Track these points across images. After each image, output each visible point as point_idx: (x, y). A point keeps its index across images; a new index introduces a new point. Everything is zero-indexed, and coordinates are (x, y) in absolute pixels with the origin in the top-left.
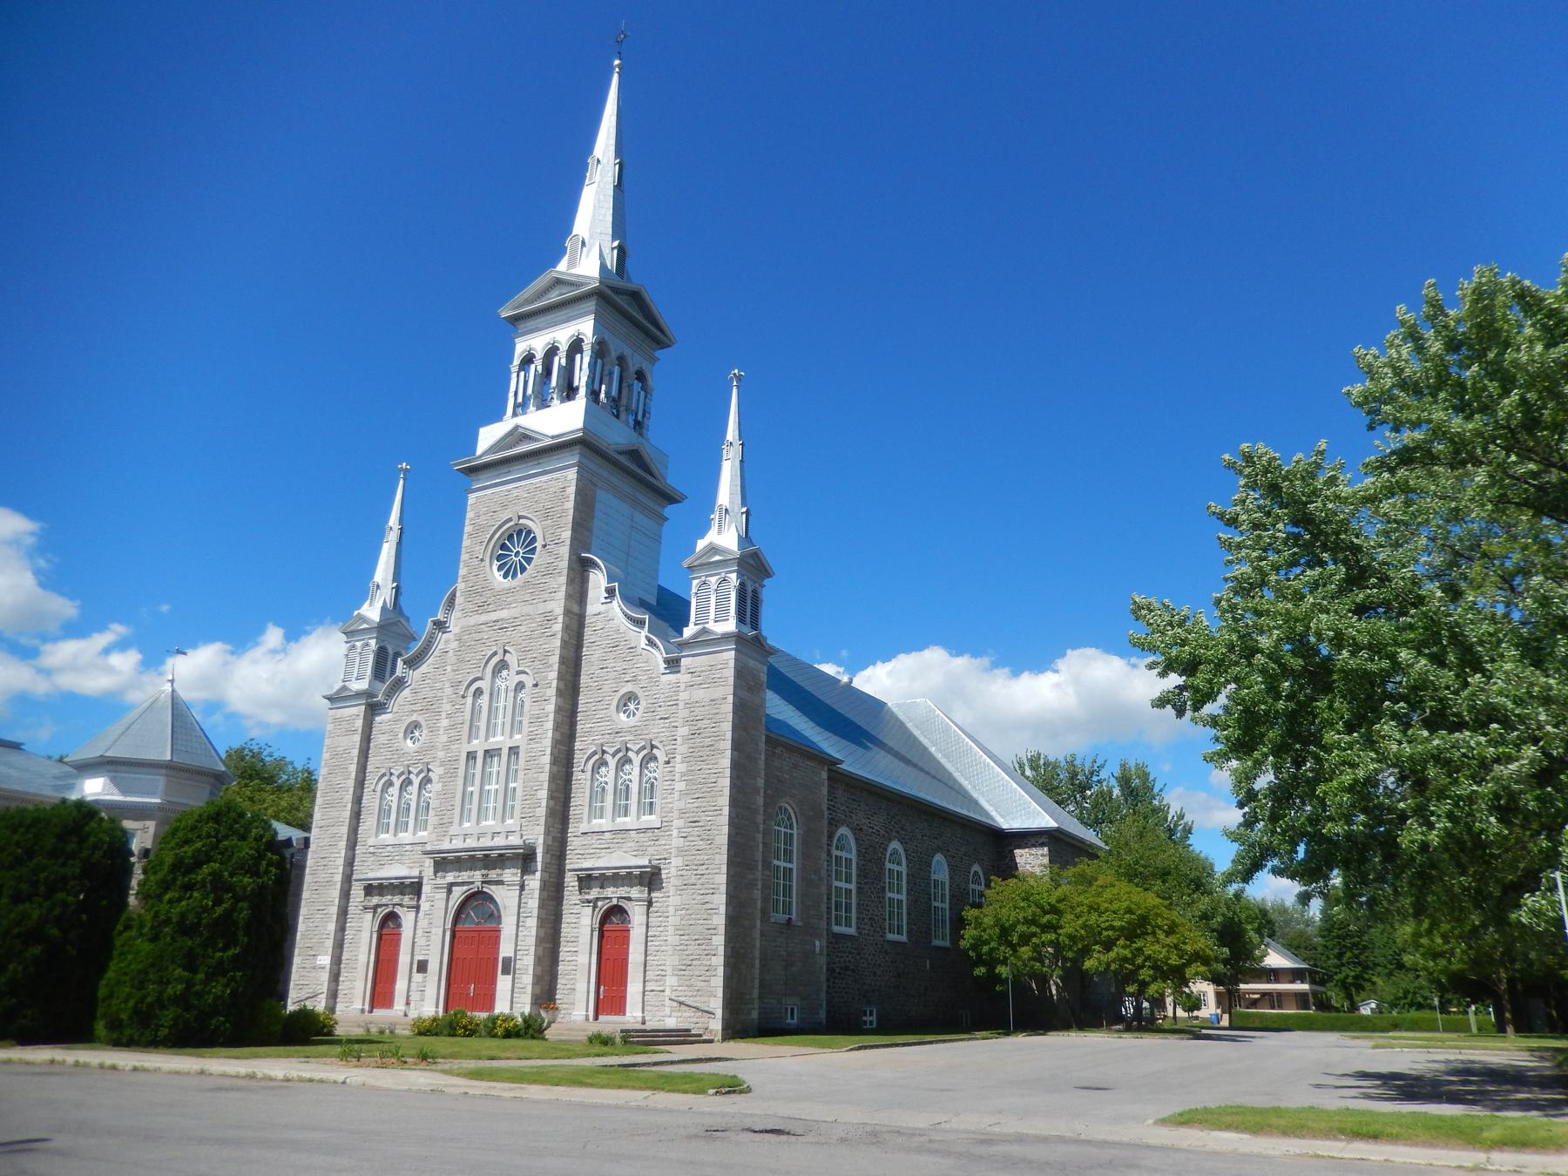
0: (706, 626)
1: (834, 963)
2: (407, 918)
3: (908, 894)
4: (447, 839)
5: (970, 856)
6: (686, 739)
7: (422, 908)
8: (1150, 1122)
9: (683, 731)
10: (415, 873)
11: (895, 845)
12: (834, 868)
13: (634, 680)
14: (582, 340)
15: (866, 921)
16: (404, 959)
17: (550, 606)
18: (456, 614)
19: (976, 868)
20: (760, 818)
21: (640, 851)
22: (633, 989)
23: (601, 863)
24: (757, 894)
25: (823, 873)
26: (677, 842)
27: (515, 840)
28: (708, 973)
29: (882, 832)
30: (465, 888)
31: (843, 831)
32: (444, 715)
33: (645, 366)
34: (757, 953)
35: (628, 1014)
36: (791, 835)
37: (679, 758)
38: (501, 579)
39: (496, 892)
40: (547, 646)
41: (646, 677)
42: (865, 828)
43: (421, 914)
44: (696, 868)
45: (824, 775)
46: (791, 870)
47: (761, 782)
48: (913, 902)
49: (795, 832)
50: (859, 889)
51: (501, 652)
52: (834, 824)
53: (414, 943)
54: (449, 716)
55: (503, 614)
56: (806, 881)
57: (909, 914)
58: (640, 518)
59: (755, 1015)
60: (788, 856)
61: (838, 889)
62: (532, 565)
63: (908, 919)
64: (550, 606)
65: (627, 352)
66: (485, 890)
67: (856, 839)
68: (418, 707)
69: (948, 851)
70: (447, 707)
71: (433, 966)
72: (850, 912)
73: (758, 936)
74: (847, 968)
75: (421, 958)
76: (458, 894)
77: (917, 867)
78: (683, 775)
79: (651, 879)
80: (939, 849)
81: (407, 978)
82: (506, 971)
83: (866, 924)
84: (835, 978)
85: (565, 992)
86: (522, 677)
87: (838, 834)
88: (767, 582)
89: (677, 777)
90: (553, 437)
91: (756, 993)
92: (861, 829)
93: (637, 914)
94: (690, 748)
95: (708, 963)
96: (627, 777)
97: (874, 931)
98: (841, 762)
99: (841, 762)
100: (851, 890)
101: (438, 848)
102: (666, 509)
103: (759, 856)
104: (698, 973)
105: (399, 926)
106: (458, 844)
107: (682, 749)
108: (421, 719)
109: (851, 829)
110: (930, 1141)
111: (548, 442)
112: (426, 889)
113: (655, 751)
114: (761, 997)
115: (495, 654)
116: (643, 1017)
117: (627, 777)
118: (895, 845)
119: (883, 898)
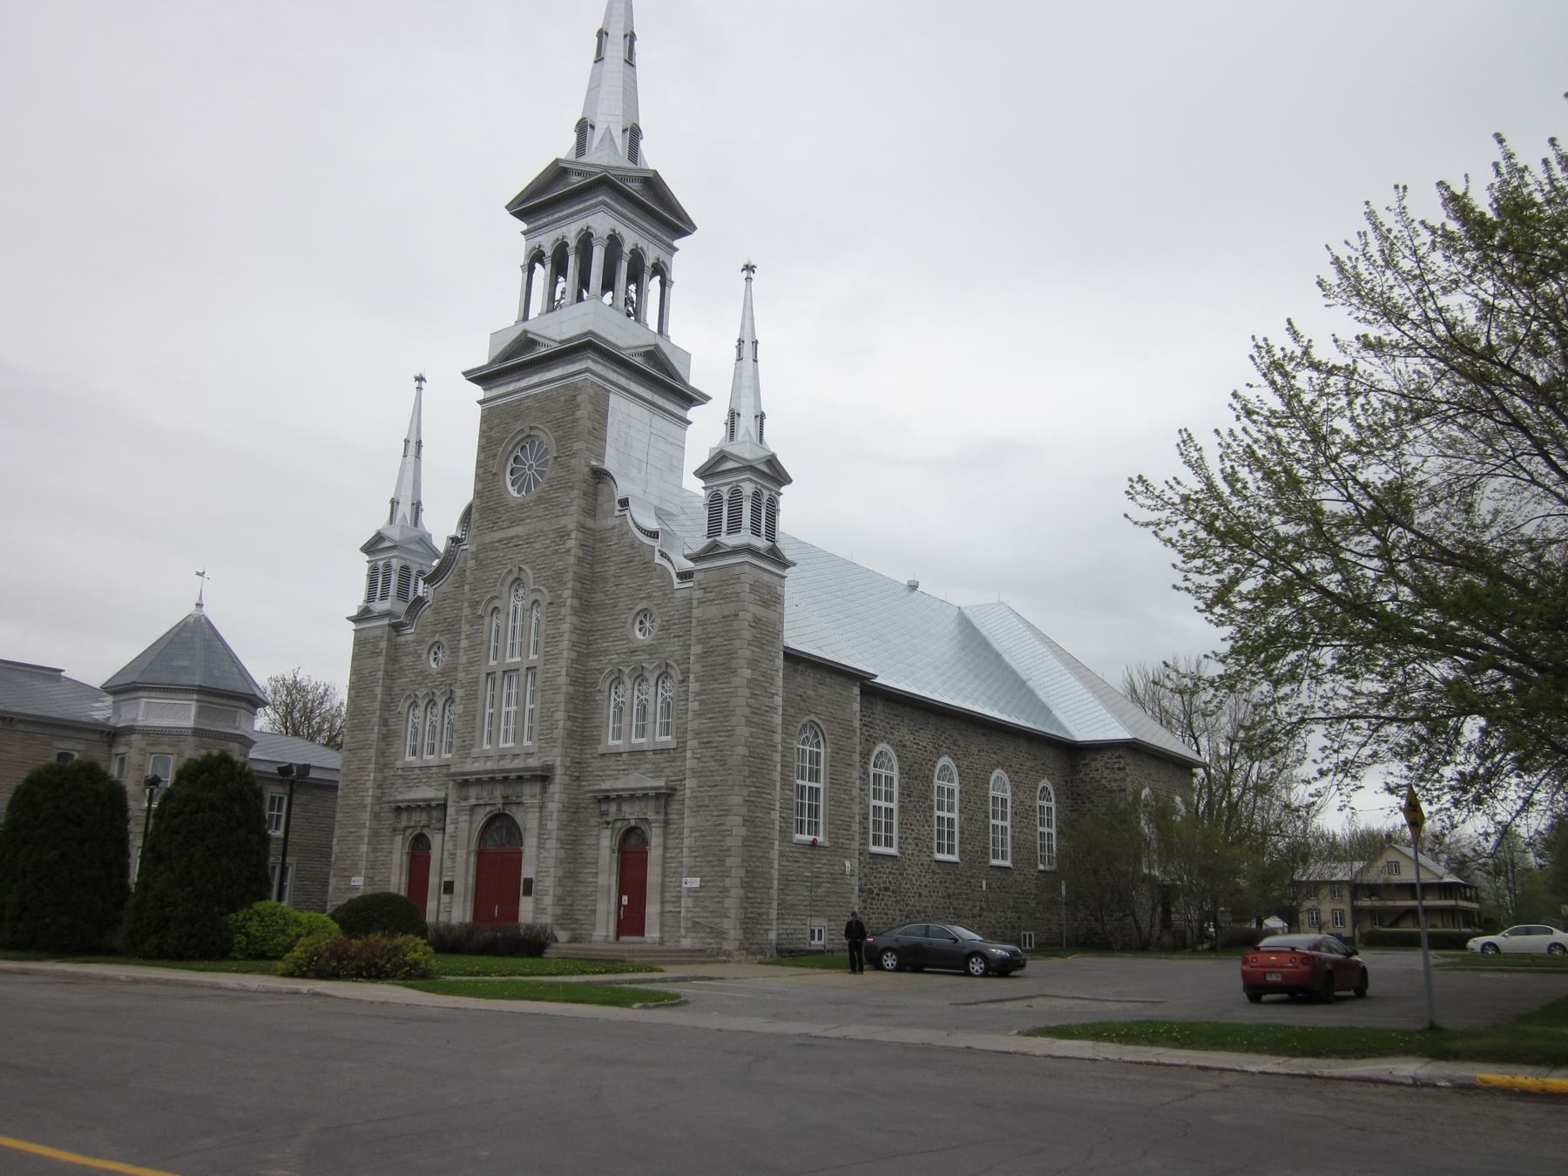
0: (718, 538)
1: (872, 884)
2: (436, 841)
3: (961, 811)
4: (469, 761)
5: (1037, 771)
6: (700, 658)
7: (447, 831)
8: (1015, 1032)
9: (696, 649)
10: (442, 794)
11: (945, 760)
12: (872, 787)
13: (649, 597)
14: (567, 244)
15: (910, 840)
16: (433, 880)
17: (564, 521)
18: (1466, 311)
19: (1045, 783)
20: (778, 738)
21: (657, 772)
22: (652, 910)
23: (619, 784)
24: (775, 815)
25: (855, 792)
26: (690, 763)
27: (533, 762)
28: (721, 895)
29: (930, 748)
30: (488, 809)
31: (882, 747)
32: (463, 636)
33: (663, 257)
34: (775, 874)
35: (646, 935)
36: (818, 754)
37: (692, 677)
38: (515, 494)
39: (518, 815)
40: (561, 563)
41: (660, 593)
42: (908, 744)
43: (447, 836)
44: (709, 789)
45: (856, 691)
46: (817, 790)
47: (779, 700)
48: (968, 820)
49: (822, 751)
50: (902, 808)
51: (516, 570)
52: (870, 741)
53: (441, 864)
54: (468, 637)
55: (519, 530)
56: (836, 803)
57: (962, 832)
58: (660, 423)
59: (773, 936)
60: (815, 775)
61: (877, 809)
62: (545, 479)
63: (961, 838)
64: (564, 521)
65: (643, 244)
66: (507, 812)
67: (898, 756)
68: (440, 627)
69: (1010, 766)
70: (465, 628)
71: (459, 887)
72: (891, 831)
73: (776, 857)
74: (887, 889)
75: (447, 879)
76: (481, 818)
77: (972, 783)
78: (697, 694)
79: (665, 797)
80: (999, 765)
81: (436, 898)
82: (528, 892)
83: (909, 844)
84: (873, 899)
85: (587, 913)
86: (538, 596)
87: (876, 752)
88: (783, 489)
89: (691, 697)
90: (562, 342)
91: (774, 914)
92: (904, 746)
93: (655, 839)
94: (703, 666)
95: (722, 885)
96: (644, 697)
97: (920, 851)
98: (876, 676)
99: (876, 676)
100: (891, 810)
101: (460, 770)
102: (689, 412)
103: (777, 776)
104: (711, 894)
105: (429, 847)
106: (477, 766)
107: (695, 668)
108: (442, 639)
109: (892, 746)
110: (1307, 1086)
111: (555, 347)
112: (451, 810)
113: (669, 670)
114: (780, 916)
115: (511, 571)
116: (661, 938)
117: (644, 697)
118: (945, 760)
119: (931, 816)
